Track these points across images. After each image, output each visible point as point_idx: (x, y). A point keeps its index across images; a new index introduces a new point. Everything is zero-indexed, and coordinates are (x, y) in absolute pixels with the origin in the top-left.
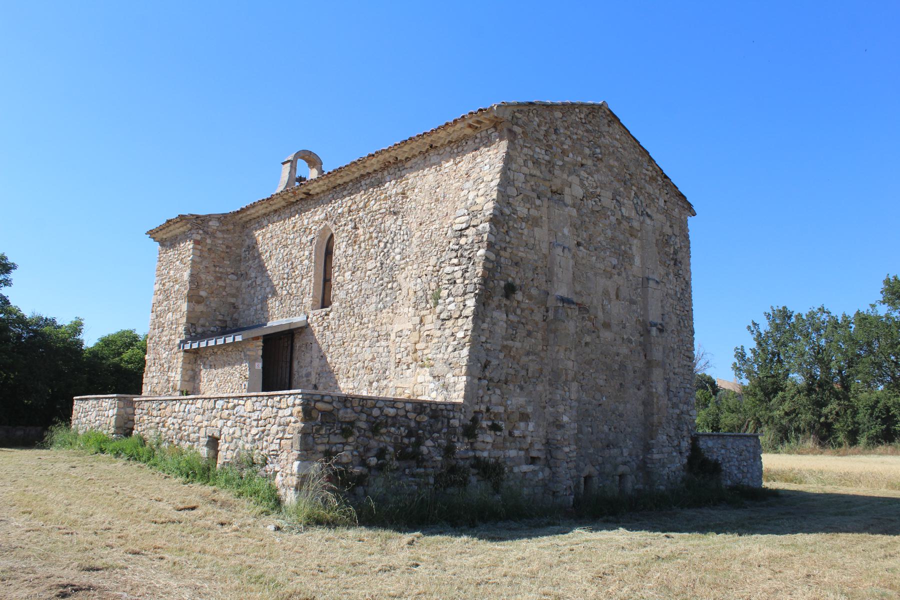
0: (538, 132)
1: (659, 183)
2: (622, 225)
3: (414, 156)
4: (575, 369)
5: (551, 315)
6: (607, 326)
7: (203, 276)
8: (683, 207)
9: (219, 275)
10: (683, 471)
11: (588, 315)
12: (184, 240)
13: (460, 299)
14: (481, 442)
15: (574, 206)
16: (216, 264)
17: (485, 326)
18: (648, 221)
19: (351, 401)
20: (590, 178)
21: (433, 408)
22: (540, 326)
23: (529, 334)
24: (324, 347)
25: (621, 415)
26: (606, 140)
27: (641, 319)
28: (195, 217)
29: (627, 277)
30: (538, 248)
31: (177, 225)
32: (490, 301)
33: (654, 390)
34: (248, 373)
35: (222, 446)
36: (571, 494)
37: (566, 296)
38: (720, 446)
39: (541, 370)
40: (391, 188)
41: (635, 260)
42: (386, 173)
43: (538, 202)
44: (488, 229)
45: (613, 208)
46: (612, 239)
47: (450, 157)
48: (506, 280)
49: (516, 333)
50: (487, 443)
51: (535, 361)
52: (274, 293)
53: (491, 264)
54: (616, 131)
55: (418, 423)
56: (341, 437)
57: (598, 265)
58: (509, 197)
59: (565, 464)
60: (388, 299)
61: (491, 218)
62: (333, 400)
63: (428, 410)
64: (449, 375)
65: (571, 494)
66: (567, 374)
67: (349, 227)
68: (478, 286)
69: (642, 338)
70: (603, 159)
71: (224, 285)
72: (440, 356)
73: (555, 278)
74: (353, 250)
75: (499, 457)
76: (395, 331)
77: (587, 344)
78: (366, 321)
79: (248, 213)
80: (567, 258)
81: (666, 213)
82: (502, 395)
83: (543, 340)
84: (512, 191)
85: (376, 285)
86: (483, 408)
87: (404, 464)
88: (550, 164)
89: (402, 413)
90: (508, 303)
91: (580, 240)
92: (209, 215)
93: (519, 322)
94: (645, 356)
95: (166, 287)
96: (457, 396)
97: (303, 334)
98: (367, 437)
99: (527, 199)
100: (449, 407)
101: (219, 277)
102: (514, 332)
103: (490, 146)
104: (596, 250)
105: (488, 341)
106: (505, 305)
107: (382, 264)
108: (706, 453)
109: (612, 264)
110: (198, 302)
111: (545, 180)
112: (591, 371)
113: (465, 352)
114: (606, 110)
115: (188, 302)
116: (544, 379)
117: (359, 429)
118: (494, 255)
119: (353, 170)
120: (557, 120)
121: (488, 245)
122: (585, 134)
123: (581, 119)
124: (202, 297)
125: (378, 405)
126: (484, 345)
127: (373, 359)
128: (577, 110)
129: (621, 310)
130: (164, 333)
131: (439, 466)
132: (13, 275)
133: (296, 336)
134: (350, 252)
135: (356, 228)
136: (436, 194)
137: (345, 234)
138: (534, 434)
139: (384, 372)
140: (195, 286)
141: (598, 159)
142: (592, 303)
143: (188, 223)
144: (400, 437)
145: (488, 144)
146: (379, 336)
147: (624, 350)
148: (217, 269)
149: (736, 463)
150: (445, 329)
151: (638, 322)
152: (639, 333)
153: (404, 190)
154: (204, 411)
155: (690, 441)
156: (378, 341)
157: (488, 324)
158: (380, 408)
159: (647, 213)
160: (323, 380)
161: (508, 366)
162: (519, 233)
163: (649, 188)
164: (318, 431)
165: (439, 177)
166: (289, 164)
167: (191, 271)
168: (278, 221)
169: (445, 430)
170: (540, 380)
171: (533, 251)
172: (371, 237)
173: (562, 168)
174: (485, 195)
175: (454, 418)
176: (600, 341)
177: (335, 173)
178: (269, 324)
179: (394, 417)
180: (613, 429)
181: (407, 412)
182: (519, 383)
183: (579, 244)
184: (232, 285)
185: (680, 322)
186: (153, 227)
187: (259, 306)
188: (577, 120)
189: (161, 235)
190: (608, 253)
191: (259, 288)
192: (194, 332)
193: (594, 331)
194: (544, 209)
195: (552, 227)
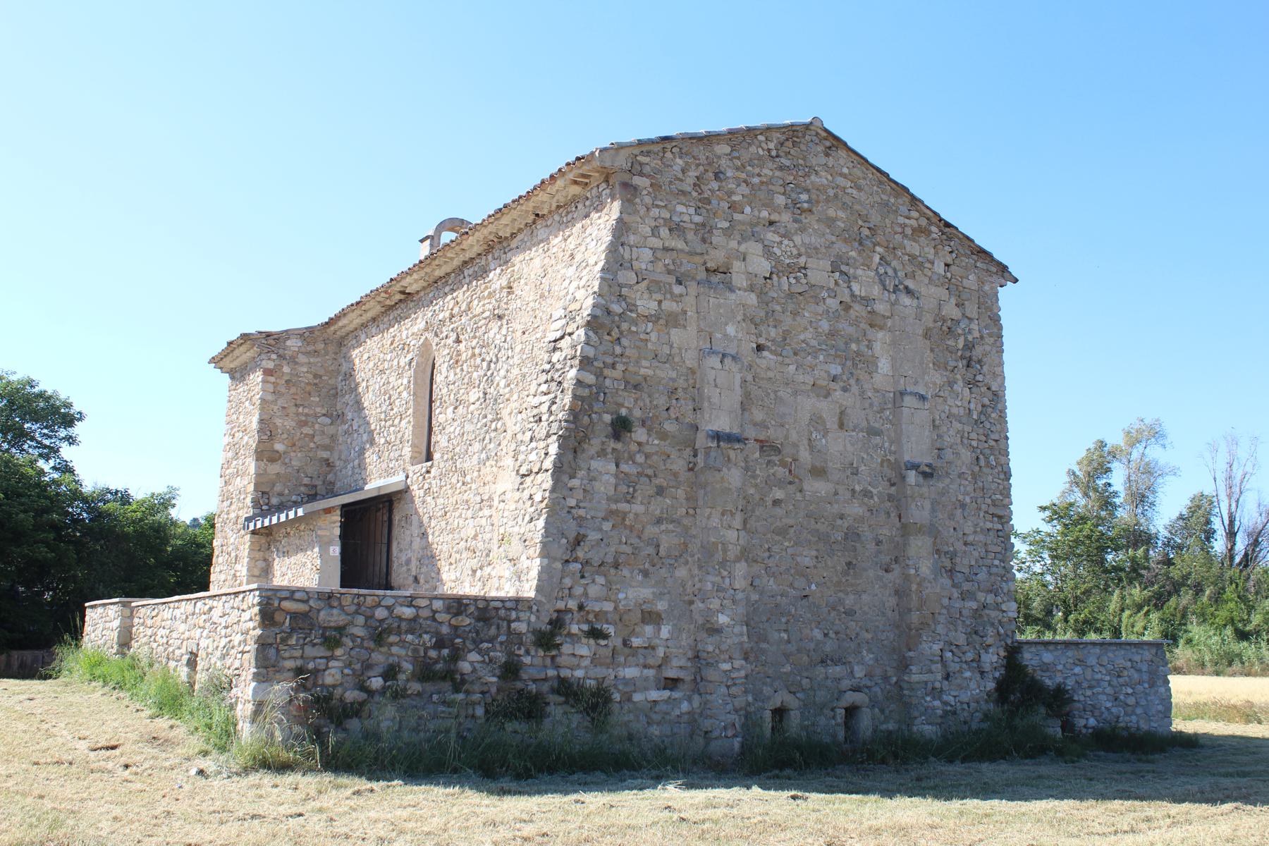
0: (681, 180)
1: (934, 236)
2: (852, 311)
3: (520, 230)
4: (741, 542)
5: (700, 460)
6: (819, 472)
7: (278, 422)
8: (988, 270)
9: (304, 418)
10: (987, 701)
11: (780, 457)
12: (253, 370)
13: (542, 444)
14: (569, 655)
15: (751, 289)
16: (298, 402)
17: (575, 483)
18: (906, 300)
19: (339, 598)
20: (786, 242)
21: (481, 606)
22: (682, 478)
23: (660, 491)
24: (425, 520)
25: (850, 613)
26: (823, 179)
27: (892, 459)
28: (264, 335)
29: (862, 393)
30: (677, 359)
31: (242, 349)
32: (586, 446)
33: (912, 572)
34: (319, 562)
35: (201, 665)
36: (735, 736)
37: (728, 430)
38: (1071, 661)
39: (685, 545)
40: (496, 278)
41: (880, 365)
42: (490, 257)
43: (678, 290)
44: (583, 338)
45: (832, 285)
46: (832, 334)
47: (559, 230)
48: (617, 413)
49: (635, 491)
50: (582, 657)
51: (673, 532)
52: (372, 442)
53: (587, 391)
54: (842, 162)
55: (456, 628)
56: (322, 649)
57: (801, 378)
58: (621, 286)
59: (723, 690)
60: (492, 446)
61: (588, 322)
62: (309, 598)
63: (472, 609)
64: (523, 558)
65: (735, 736)
66: (725, 551)
67: (450, 341)
68: (563, 423)
69: (893, 488)
70: (814, 209)
71: (311, 432)
72: (516, 529)
73: (706, 404)
74: (455, 374)
75: (604, 678)
76: (498, 493)
77: (776, 503)
78: (469, 481)
79: (340, 324)
80: (730, 371)
81: (952, 286)
82: (609, 585)
83: (687, 499)
84: (627, 277)
85: (479, 425)
86: (572, 604)
87: (429, 687)
88: (704, 231)
89: (425, 613)
90: (619, 446)
91: (762, 341)
92: (286, 331)
93: (639, 474)
94: (900, 517)
95: (236, 439)
96: (529, 590)
97: (403, 502)
98: (366, 649)
99: (654, 287)
100: (508, 605)
101: (302, 421)
102: (631, 489)
103: (601, 211)
104: (795, 354)
105: (581, 505)
106: (613, 449)
107: (485, 394)
108: (1039, 672)
109: (829, 375)
110: (272, 460)
111: (692, 253)
112: (786, 544)
113: (541, 523)
114: (820, 131)
115: (257, 460)
116: (690, 559)
117: (353, 637)
118: (592, 377)
119: (449, 255)
120: (719, 157)
121: (581, 362)
122: (778, 173)
123: (769, 150)
124: (277, 452)
125: (383, 603)
126: (573, 511)
127: (476, 536)
128: (761, 138)
129: (848, 445)
130: (233, 507)
131: (494, 690)
132: (78, 429)
133: (396, 504)
134: (451, 378)
135: (458, 341)
136: (542, 286)
137: (447, 351)
138: (670, 644)
139: (488, 555)
140: (266, 437)
141: (803, 211)
142: (786, 437)
143: (254, 345)
144: (422, 650)
145: (599, 208)
146: (482, 501)
147: (856, 509)
148: (300, 410)
149: (1109, 690)
150: (524, 489)
151: (885, 464)
152: (889, 480)
153: (509, 283)
154: (187, 617)
155: (1002, 653)
156: (481, 509)
157: (582, 479)
158: (388, 608)
159: (906, 288)
160: (424, 569)
161: (620, 542)
162: (642, 340)
163: (912, 247)
164: (284, 640)
165: (547, 260)
166: (428, 242)
167: (260, 414)
168: (377, 334)
169: (502, 638)
170: (682, 560)
171: (667, 365)
172: (474, 355)
173: (728, 232)
174: (586, 287)
175: (518, 619)
176: (804, 497)
177: (428, 261)
178: (367, 488)
179: (415, 619)
180: (832, 635)
181: (435, 612)
182: (642, 567)
183: (760, 348)
184: (323, 432)
185: (978, 458)
186: (215, 353)
187: (356, 462)
188: (761, 152)
189: (227, 363)
190: (821, 358)
191: (356, 435)
192: (267, 504)
193: (793, 480)
194: (690, 301)
195: (702, 325)
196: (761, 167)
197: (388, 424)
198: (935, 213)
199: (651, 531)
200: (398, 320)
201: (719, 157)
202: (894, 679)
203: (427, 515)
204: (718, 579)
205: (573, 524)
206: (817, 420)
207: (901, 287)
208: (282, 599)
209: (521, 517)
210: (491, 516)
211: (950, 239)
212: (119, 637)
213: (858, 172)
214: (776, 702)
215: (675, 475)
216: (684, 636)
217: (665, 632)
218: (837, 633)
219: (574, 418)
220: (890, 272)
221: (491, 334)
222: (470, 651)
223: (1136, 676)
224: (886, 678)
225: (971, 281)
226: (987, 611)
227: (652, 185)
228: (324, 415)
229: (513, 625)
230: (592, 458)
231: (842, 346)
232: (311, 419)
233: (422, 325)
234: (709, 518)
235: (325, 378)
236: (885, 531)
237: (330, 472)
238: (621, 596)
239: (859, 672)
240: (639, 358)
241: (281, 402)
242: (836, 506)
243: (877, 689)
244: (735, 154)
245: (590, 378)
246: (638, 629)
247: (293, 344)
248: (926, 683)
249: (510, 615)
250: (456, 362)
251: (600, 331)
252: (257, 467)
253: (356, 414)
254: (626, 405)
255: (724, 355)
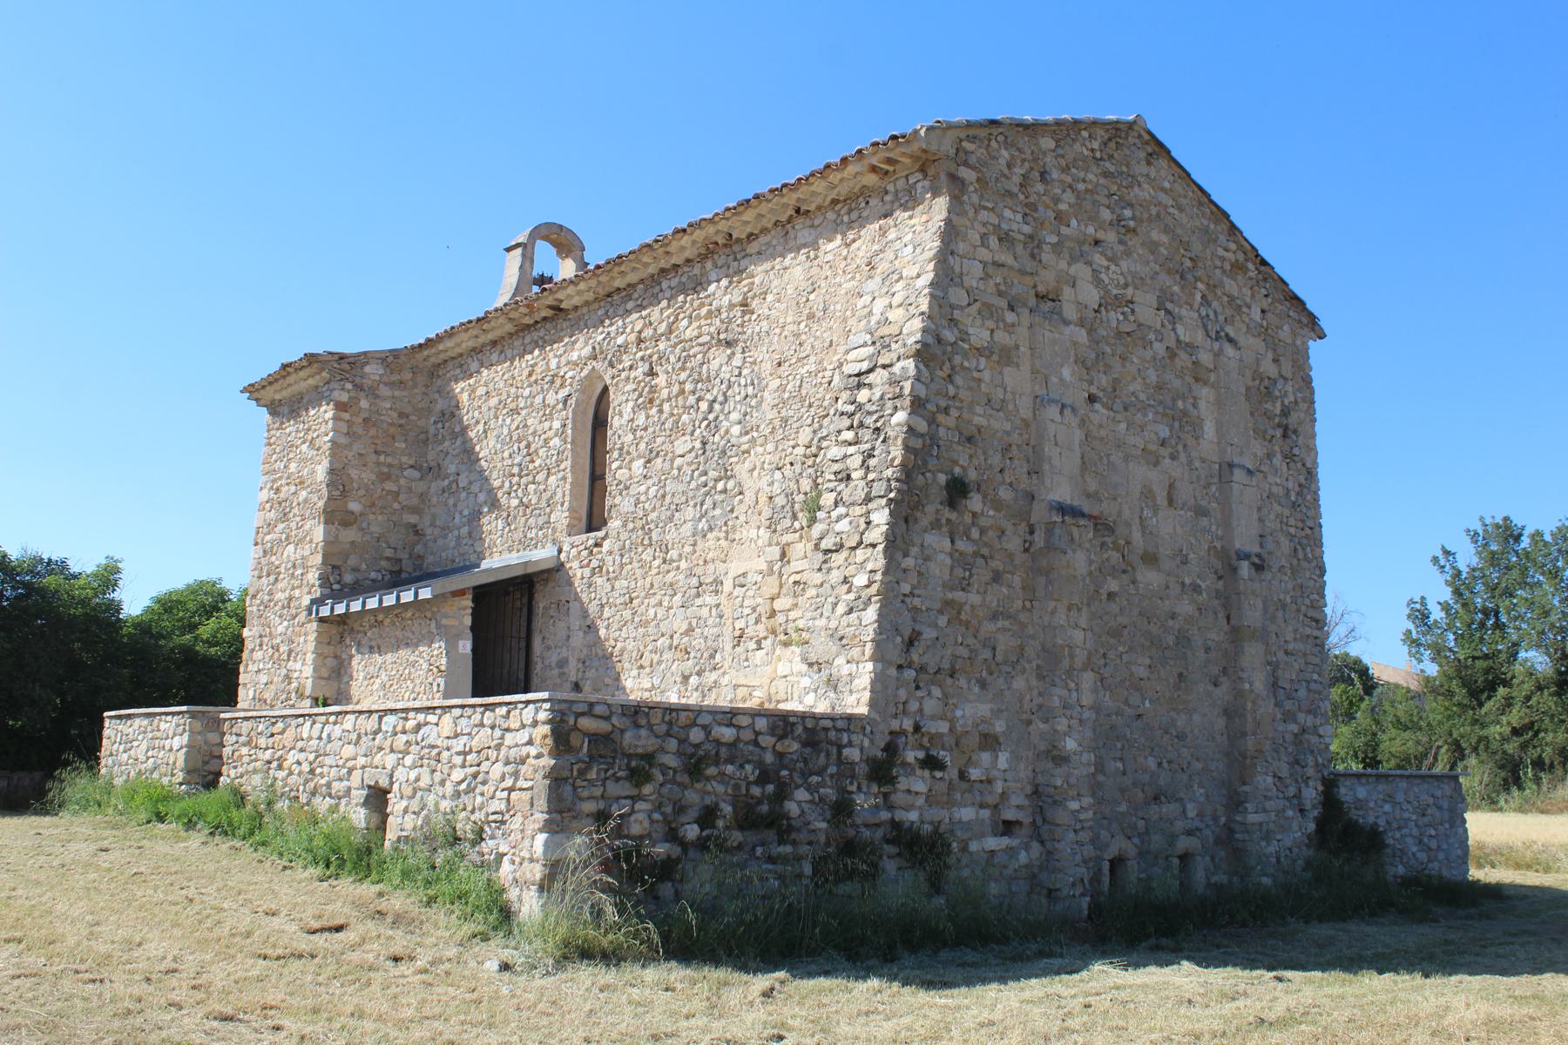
0: (1007, 178)
2: (1177, 360)
3: (764, 231)
5: (1039, 539)
6: (1151, 559)
7: (354, 473)
9: (386, 470)
13: (858, 510)
15: (1081, 323)
16: (380, 448)
17: (909, 562)
18: (1229, 350)
19: (647, 714)
20: (1113, 267)
21: (809, 726)
23: (997, 577)
25: (1181, 737)
26: (1143, 192)
27: (1218, 545)
28: (336, 357)
29: (1190, 463)
30: (1011, 407)
32: (919, 514)
33: (1247, 686)
34: (444, 661)
35: (396, 805)
36: (1083, 895)
37: (1069, 502)
38: (1381, 796)
39: (1022, 648)
40: (721, 293)
41: (1206, 428)
42: (709, 265)
43: (1010, 317)
46: (1159, 387)
47: (836, 232)
49: (971, 576)
50: (917, 793)
52: (494, 504)
53: (920, 441)
54: (1163, 173)
55: (780, 755)
56: (627, 784)
58: (952, 307)
59: (1072, 835)
60: (718, 512)
61: (918, 351)
63: (799, 730)
65: (1083, 895)
66: (1072, 656)
68: (893, 484)
69: (1221, 582)
72: (821, 623)
73: (1046, 467)
74: (648, 417)
75: (940, 822)
76: (731, 575)
77: (1111, 596)
78: (675, 557)
79: (441, 347)
83: (1023, 588)
84: (958, 296)
87: (752, 837)
89: (747, 735)
90: (953, 516)
91: (1094, 390)
92: (365, 353)
93: (976, 554)
94: (1228, 618)
95: (282, 495)
97: (551, 585)
99: (988, 311)
100: (840, 724)
101: (383, 474)
103: (913, 209)
105: (916, 592)
107: (704, 443)
108: (1353, 811)
110: (346, 524)
111: (1022, 272)
112: (1121, 649)
113: (871, 614)
115: (326, 523)
116: (1027, 666)
117: (664, 769)
120: (1044, 153)
121: (912, 403)
122: (1102, 181)
123: (1093, 150)
124: (352, 513)
126: (908, 600)
128: (1085, 134)
129: (1178, 527)
130: (280, 585)
131: (823, 839)
135: (652, 373)
138: (1009, 775)
139: (712, 656)
141: (1129, 230)
142: (1120, 514)
143: (323, 369)
144: (743, 784)
146: (701, 585)
147: (1186, 608)
148: (382, 458)
149: (1415, 832)
150: (830, 569)
153: (745, 298)
155: (1321, 788)
156: (698, 595)
158: (704, 727)
159: (1227, 335)
160: (591, 674)
163: (1231, 286)
164: (582, 773)
165: (815, 270)
166: (519, 251)
167: (331, 462)
168: (499, 363)
169: (832, 769)
170: (1019, 667)
171: (1001, 414)
172: (682, 392)
173: (1057, 248)
175: (850, 744)
177: (609, 266)
178: (485, 565)
179: (733, 745)
180: (1165, 765)
181: (757, 734)
183: (1092, 399)
184: (410, 488)
186: (255, 378)
187: (465, 530)
190: (1150, 416)
191: (464, 495)
192: (339, 583)
193: (1126, 569)
194: (1023, 331)
196: (1087, 170)
197: (524, 480)
198: (1253, 247)
199: (988, 627)
200: (541, 344)
201: (1044, 153)
202: (1223, 820)
203: (596, 602)
204: (1064, 693)
205: (907, 616)
206: (1148, 494)
207: (1223, 334)
208: (579, 715)
209: (828, 607)
210: (718, 606)
211: (1265, 280)
212: (186, 760)
213: (1178, 188)
214: (1112, 851)
215: (1011, 556)
216: (1022, 766)
217: (1003, 760)
218: (1169, 762)
219: (907, 476)
220: (1212, 316)
221: (715, 364)
222: (798, 787)
223: (1438, 814)
224: (1215, 818)
225: (1285, 333)
226: (1307, 736)
227: (978, 180)
228: (412, 467)
229: (846, 752)
230: (925, 532)
231: (1170, 403)
232: (395, 471)
233: (587, 351)
234: (1053, 613)
235: (413, 418)
236: (1214, 636)
237: (418, 542)
238: (959, 713)
239: (1192, 811)
240: (972, 402)
241: (357, 447)
242: (1167, 602)
243: (1207, 832)
244: (1060, 151)
245: (922, 426)
246: (974, 758)
247: (373, 370)
248: (1261, 824)
249: (841, 739)
250: (649, 400)
251: (932, 364)
252: (326, 533)
253: (463, 467)
254: (961, 462)
255: (1063, 406)
